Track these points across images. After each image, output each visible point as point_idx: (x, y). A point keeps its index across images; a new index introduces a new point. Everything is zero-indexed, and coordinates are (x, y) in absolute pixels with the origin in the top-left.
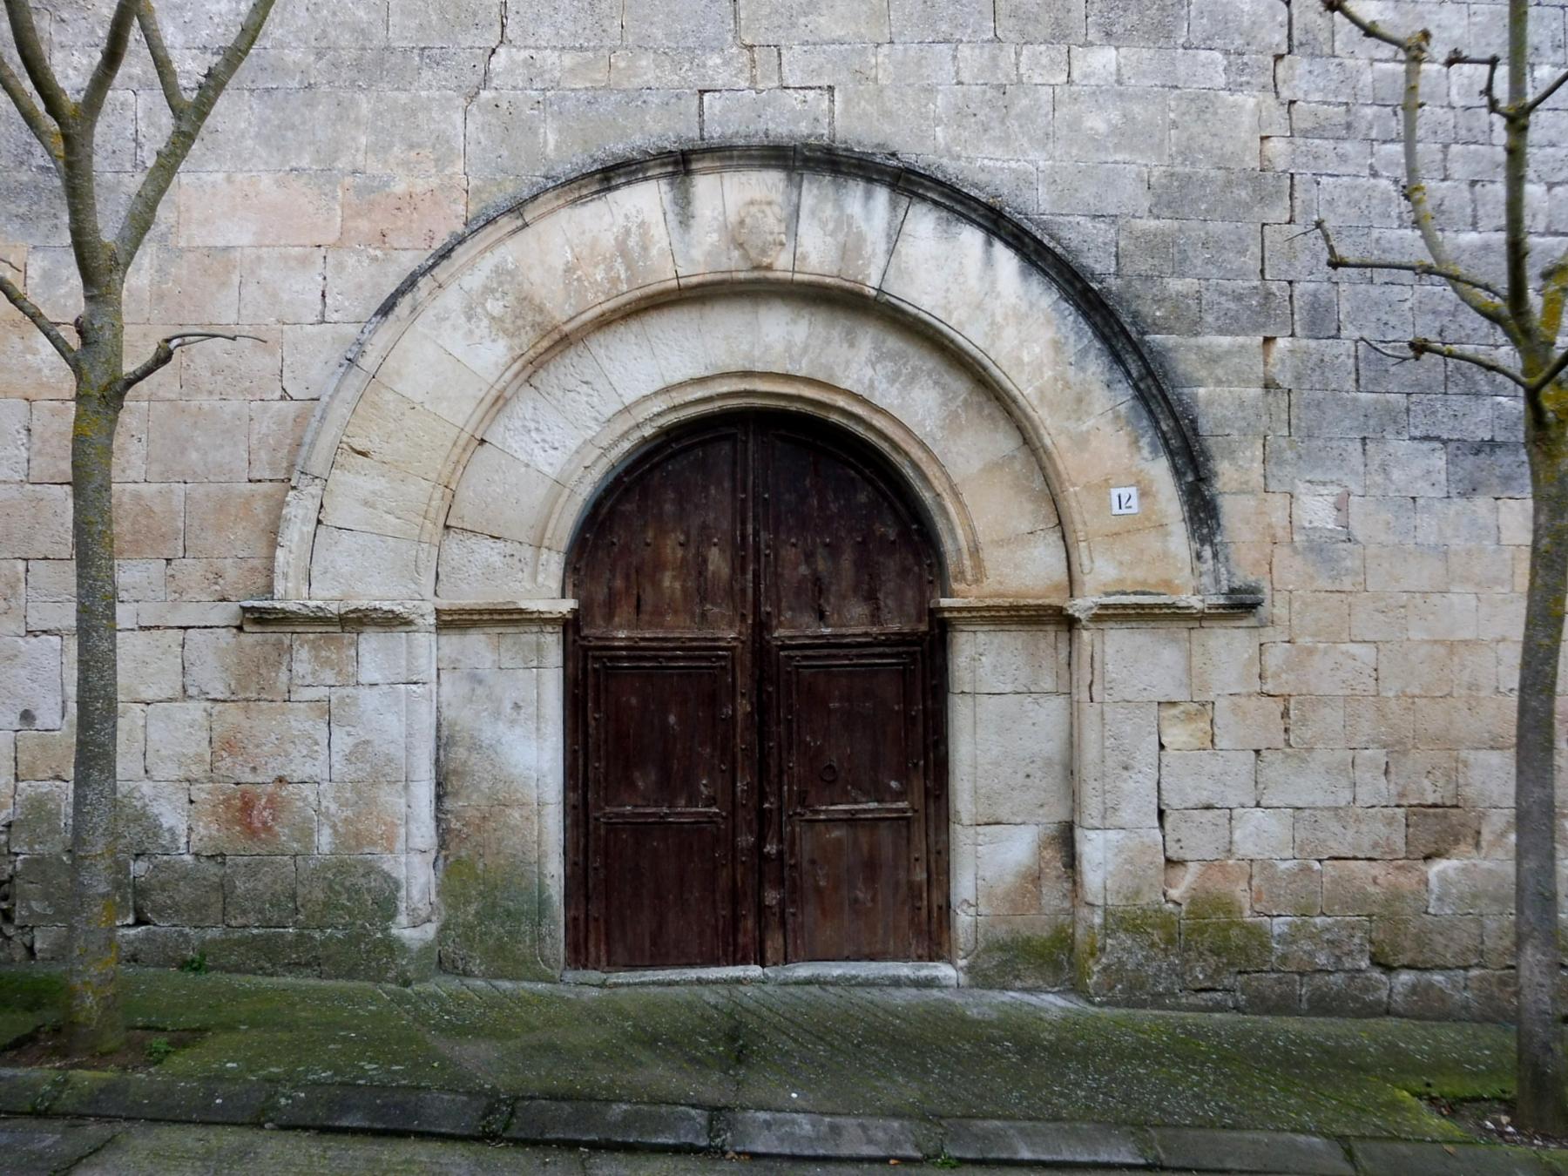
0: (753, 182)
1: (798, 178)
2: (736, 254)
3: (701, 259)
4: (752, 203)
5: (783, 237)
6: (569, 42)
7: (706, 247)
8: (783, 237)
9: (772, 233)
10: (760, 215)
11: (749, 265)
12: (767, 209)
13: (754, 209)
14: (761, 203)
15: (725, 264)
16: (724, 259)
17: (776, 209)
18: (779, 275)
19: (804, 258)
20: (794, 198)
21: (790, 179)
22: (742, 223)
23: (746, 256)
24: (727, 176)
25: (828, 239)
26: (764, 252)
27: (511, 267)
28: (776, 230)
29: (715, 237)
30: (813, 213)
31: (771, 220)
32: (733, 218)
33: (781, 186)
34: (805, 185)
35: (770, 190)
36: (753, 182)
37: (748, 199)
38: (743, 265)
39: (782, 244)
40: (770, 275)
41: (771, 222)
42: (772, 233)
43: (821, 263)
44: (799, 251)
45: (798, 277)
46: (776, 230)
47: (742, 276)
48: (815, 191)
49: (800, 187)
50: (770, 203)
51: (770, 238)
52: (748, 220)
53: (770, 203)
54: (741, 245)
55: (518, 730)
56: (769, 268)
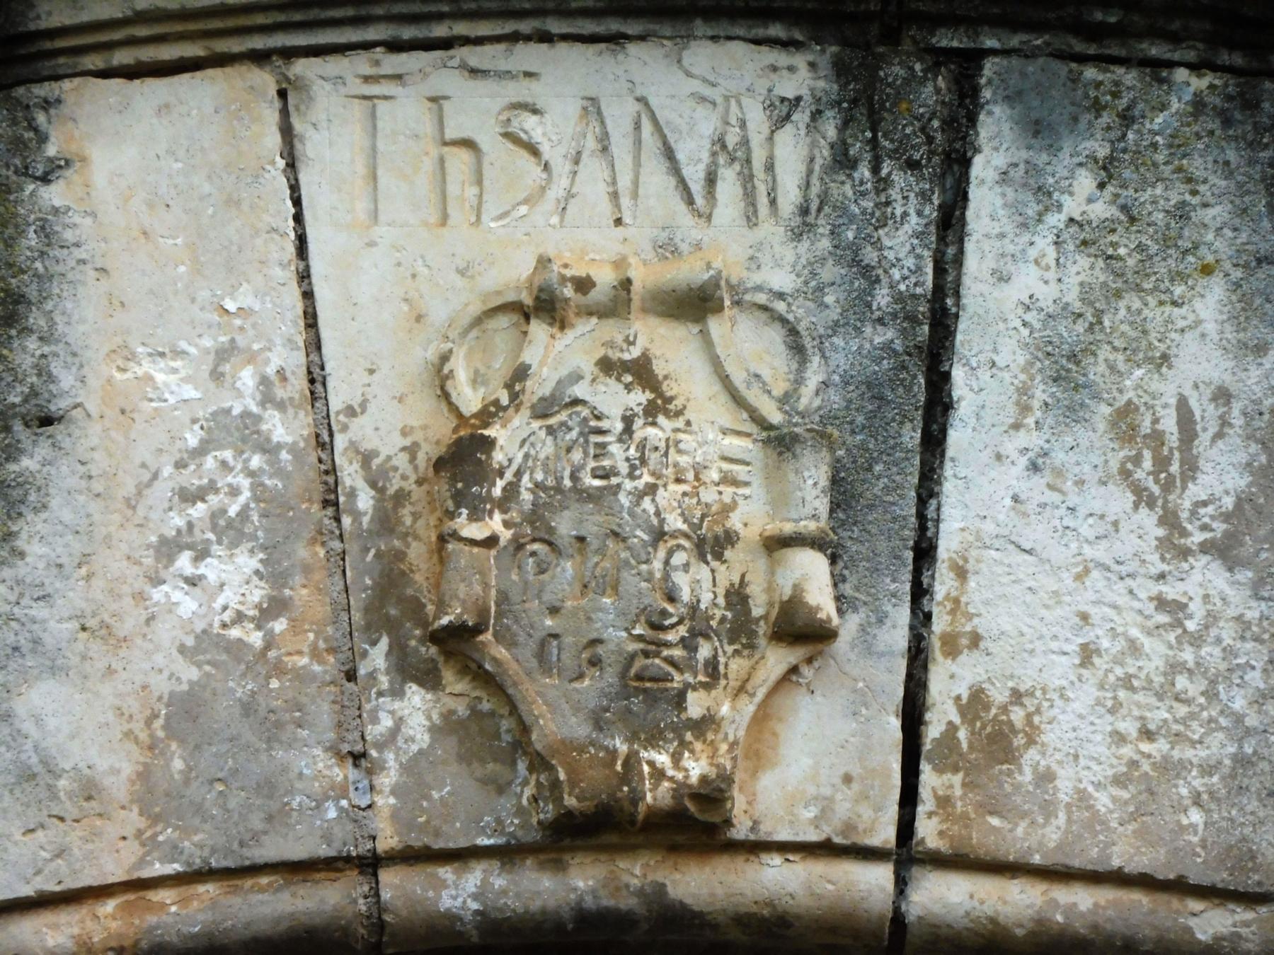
0: (554, 128)
1: (932, 93)
2: (412, 716)
3: (117, 766)
4: (544, 305)
5: (811, 575)
6: (532, 438)
7: (163, 668)
8: (811, 575)
9: (713, 544)
10: (616, 400)
11: (515, 808)
12: (672, 348)
13: (558, 355)
14: (618, 304)
15: (315, 799)
16: (315, 764)
17: (749, 346)
18: (780, 881)
19: (997, 738)
20: (904, 248)
21: (862, 105)
22: (463, 460)
23: (495, 733)
24: (332, 88)
25: (1205, 581)
26: (647, 697)
27: (1164, 369)
28: (751, 516)
29: (235, 577)
30: (1065, 368)
31: (709, 436)
32: (388, 425)
33: (792, 156)
34: (995, 152)
35: (696, 198)
36: (554, 128)
37: (512, 273)
38: (468, 805)
39: (803, 632)
40: (699, 884)
41: (715, 451)
42: (713, 544)
43: (1146, 785)
44: (947, 684)
45: (944, 896)
46: (751, 516)
47: (460, 893)
48: (1083, 197)
49: (955, 165)
50: (695, 304)
51: (700, 584)
52: (509, 440)
53: (695, 304)
54: (457, 642)
55: (411, 732)
56: (698, 824)
